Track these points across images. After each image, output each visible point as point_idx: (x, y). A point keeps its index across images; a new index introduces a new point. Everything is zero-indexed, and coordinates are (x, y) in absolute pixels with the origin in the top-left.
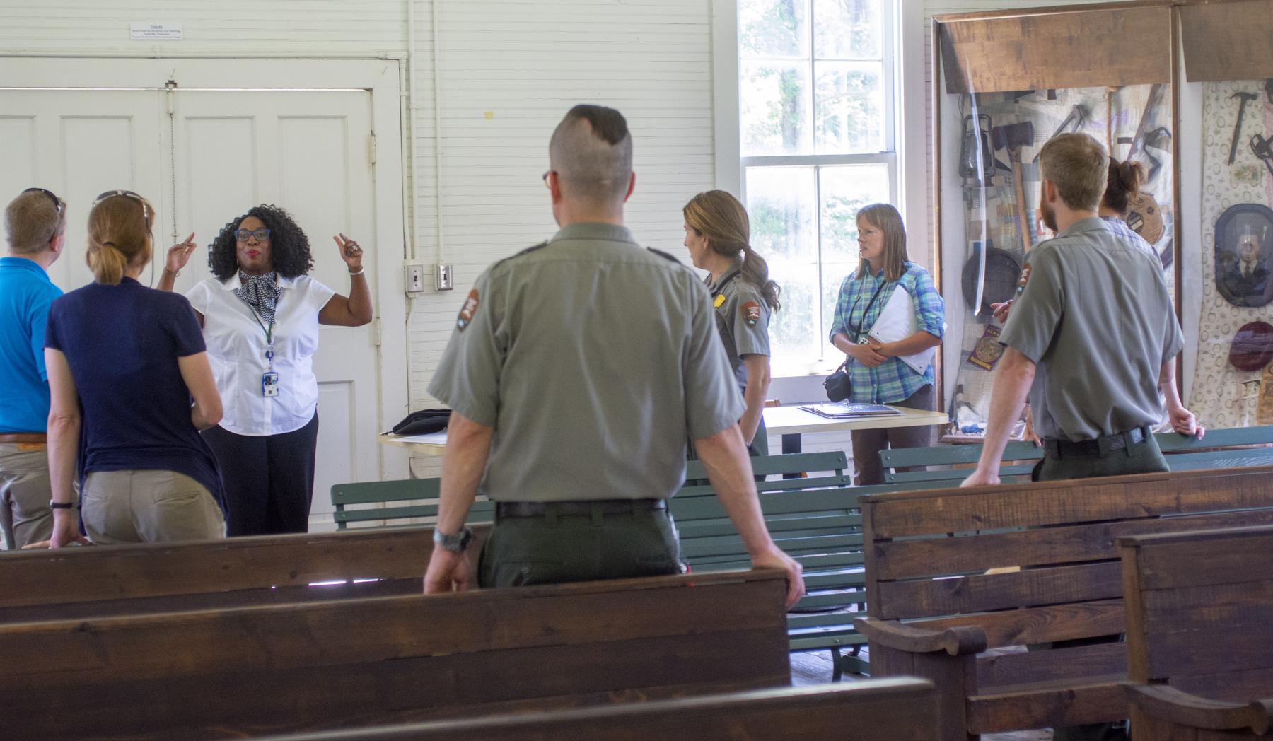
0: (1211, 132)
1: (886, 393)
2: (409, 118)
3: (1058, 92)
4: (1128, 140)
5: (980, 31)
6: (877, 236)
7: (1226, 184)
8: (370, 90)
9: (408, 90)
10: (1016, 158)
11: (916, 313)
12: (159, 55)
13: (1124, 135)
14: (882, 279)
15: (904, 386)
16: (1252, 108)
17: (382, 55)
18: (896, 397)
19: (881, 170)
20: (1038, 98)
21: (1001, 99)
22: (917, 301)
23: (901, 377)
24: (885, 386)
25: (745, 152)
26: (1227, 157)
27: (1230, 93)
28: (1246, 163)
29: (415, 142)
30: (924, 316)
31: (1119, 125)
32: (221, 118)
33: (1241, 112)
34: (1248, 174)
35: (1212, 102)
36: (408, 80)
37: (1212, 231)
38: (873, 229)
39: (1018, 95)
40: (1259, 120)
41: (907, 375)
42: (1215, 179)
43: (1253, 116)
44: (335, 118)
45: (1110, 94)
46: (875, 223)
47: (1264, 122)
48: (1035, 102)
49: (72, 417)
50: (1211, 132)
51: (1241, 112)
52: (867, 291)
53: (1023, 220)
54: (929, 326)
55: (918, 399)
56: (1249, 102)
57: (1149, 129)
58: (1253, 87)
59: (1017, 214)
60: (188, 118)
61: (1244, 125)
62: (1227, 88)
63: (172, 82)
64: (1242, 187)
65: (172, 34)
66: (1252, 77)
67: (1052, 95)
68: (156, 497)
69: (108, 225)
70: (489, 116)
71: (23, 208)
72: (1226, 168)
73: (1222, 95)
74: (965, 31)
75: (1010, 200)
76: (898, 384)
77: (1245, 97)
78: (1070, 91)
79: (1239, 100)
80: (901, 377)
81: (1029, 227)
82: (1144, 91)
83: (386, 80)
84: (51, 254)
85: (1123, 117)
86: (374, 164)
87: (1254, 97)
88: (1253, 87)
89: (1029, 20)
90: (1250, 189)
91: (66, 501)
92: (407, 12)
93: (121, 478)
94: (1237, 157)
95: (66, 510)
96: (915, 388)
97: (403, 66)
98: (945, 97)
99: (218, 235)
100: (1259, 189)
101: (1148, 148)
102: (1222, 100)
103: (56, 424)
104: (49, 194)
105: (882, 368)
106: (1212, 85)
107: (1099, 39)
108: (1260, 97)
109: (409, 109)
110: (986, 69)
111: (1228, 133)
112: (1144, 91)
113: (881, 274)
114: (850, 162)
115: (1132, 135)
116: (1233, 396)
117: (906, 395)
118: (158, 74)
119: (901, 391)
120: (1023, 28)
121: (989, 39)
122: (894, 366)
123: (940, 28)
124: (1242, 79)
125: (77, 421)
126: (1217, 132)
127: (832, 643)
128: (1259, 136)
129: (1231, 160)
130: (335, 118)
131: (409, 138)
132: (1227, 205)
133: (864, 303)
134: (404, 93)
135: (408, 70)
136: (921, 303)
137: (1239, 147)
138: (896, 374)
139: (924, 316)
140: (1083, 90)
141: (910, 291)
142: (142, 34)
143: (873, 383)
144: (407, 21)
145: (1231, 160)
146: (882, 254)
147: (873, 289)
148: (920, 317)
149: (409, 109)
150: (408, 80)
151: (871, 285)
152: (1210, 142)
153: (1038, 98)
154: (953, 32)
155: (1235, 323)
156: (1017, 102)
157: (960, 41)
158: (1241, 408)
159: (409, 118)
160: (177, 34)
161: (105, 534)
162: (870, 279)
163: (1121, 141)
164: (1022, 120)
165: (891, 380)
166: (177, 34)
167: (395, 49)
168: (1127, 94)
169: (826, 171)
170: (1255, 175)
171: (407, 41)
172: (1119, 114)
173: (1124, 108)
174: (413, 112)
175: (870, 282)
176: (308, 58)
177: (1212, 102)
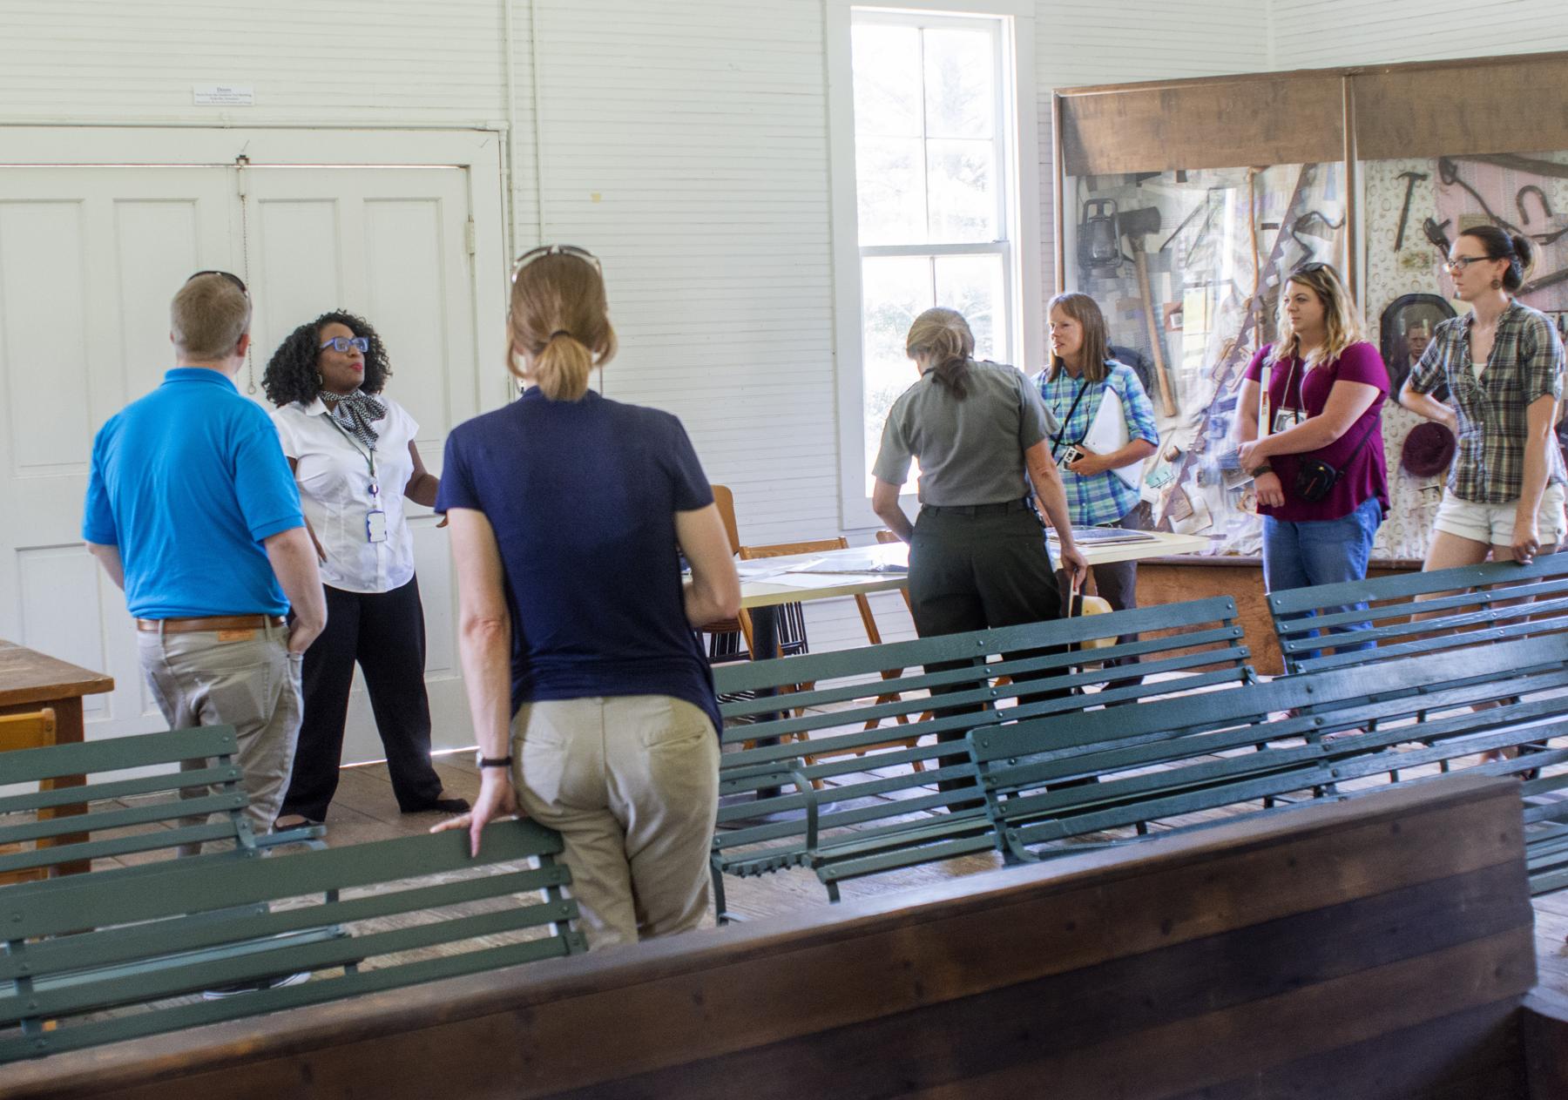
0: (1376, 216)
1: (1099, 513)
2: (510, 201)
3: (1190, 173)
4: (1274, 226)
5: (1112, 106)
6: (1075, 334)
7: (1392, 273)
8: (466, 167)
9: (509, 166)
10: (1137, 248)
11: (1126, 418)
12: (229, 124)
13: (1269, 221)
14: (1083, 380)
15: (1118, 504)
16: (1420, 190)
17: (480, 126)
18: (1109, 516)
19: (994, 262)
20: (1165, 181)
21: (1121, 183)
22: (1127, 404)
23: (1114, 494)
24: (1096, 505)
25: (865, 238)
26: (1393, 243)
27: (1396, 173)
28: (1415, 250)
29: (517, 228)
30: (1138, 422)
31: (1262, 209)
32: (298, 201)
33: (1409, 194)
34: (1418, 262)
35: (1377, 182)
36: (509, 155)
37: (1378, 324)
38: (1070, 321)
39: (1140, 178)
40: (1431, 202)
41: (1121, 491)
42: (1382, 266)
43: (1423, 198)
44: (427, 200)
45: (1253, 175)
46: (1072, 314)
47: (1437, 205)
48: (1161, 185)
49: (502, 619)
50: (1376, 216)
51: (1409, 194)
52: (1065, 395)
53: (1149, 315)
54: (1146, 433)
55: (1138, 517)
56: (1418, 183)
57: (1299, 213)
58: (1421, 166)
59: (1143, 310)
60: (262, 202)
61: (1413, 207)
62: (1392, 167)
63: (243, 157)
64: (1409, 275)
65: (241, 99)
66: (1421, 154)
67: (1181, 177)
68: (647, 741)
69: (558, 302)
70: (596, 198)
71: (204, 296)
72: (1392, 256)
73: (1388, 176)
74: (1092, 107)
75: (1134, 292)
76: (1111, 501)
77: (1414, 177)
78: (1204, 172)
79: (1406, 180)
80: (1114, 494)
81: (1156, 322)
82: (1292, 172)
83: (484, 154)
84: (237, 359)
85: (1267, 201)
86: (472, 255)
87: (1424, 177)
88: (1421, 166)
89: (1171, 92)
90: (1419, 278)
91: (503, 756)
92: (506, 75)
93: (588, 709)
94: (1405, 243)
95: (503, 769)
96: (1131, 505)
97: (504, 138)
98: (1065, 179)
99: (291, 333)
100: (1429, 278)
101: (1298, 234)
102: (1387, 183)
103: (477, 631)
104: (233, 279)
105: (1091, 485)
106: (1376, 163)
107: (1255, 113)
108: (1431, 178)
109: (510, 190)
110: (1112, 151)
111: (1395, 216)
112: (1292, 172)
113: (1081, 376)
114: (965, 252)
115: (1280, 220)
116: (1411, 505)
117: (1121, 514)
118: (226, 146)
119: (1114, 510)
120: (1163, 102)
121: (1120, 113)
122: (1106, 482)
123: (1062, 103)
124: (1411, 157)
125: (508, 624)
126: (1382, 216)
127: (1137, 817)
128: (1429, 220)
129: (1398, 246)
130: (427, 200)
131: (511, 224)
132: (1393, 296)
133: (1066, 409)
134: (505, 171)
135: (508, 144)
136: (1133, 407)
137: (1407, 232)
138: (1108, 491)
139: (1138, 422)
140: (1219, 171)
141: (1119, 394)
142: (207, 99)
143: (1081, 501)
144: (506, 85)
145: (1398, 246)
146: (1081, 350)
147: (1073, 393)
148: (1132, 423)
149: (510, 190)
150: (509, 155)
151: (1070, 389)
152: (1375, 226)
153: (1165, 181)
154: (1077, 109)
155: (1404, 425)
156: (1139, 185)
157: (1086, 117)
158: (1421, 517)
159: (510, 201)
160: (247, 99)
161: (557, 802)
162: (1068, 381)
163: (1265, 227)
164: (1146, 205)
165: (1103, 497)
166: (247, 99)
167: (494, 119)
168: (1272, 175)
169: (942, 260)
170: (1426, 262)
171: (506, 109)
172: (1262, 198)
173: (1268, 191)
174: (515, 193)
175: (1066, 384)
176: (384, 128)
177: (1377, 182)
